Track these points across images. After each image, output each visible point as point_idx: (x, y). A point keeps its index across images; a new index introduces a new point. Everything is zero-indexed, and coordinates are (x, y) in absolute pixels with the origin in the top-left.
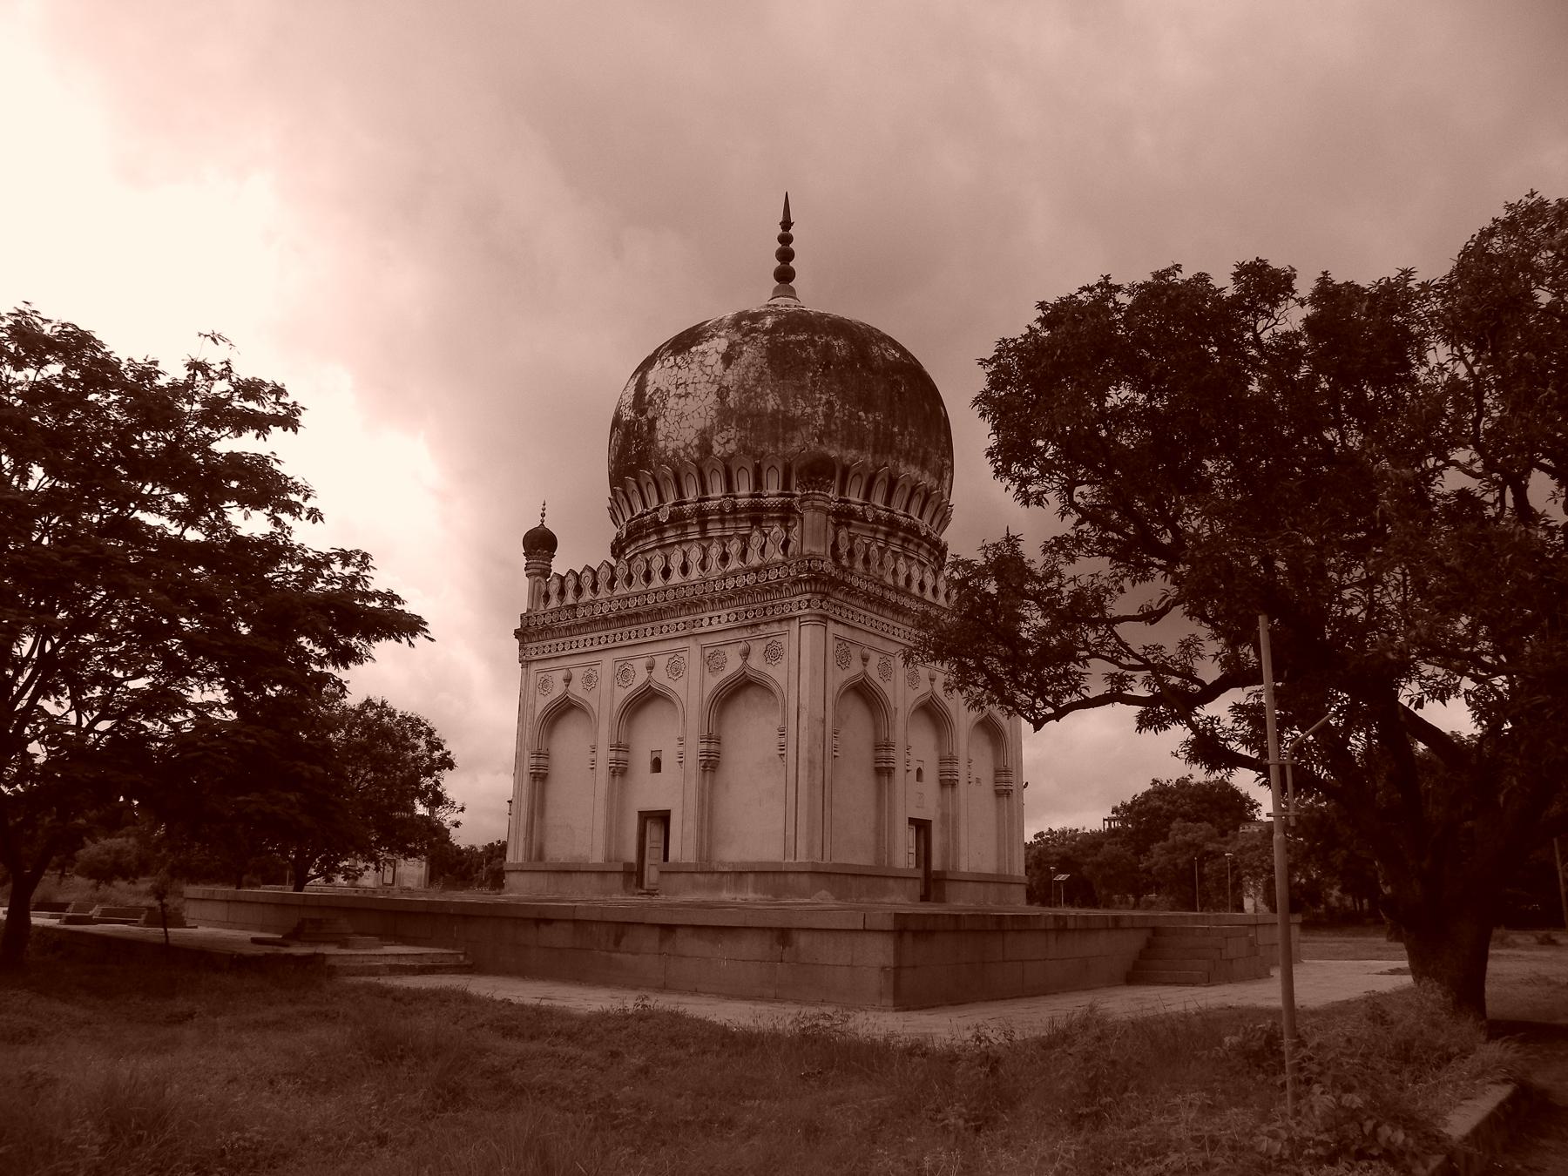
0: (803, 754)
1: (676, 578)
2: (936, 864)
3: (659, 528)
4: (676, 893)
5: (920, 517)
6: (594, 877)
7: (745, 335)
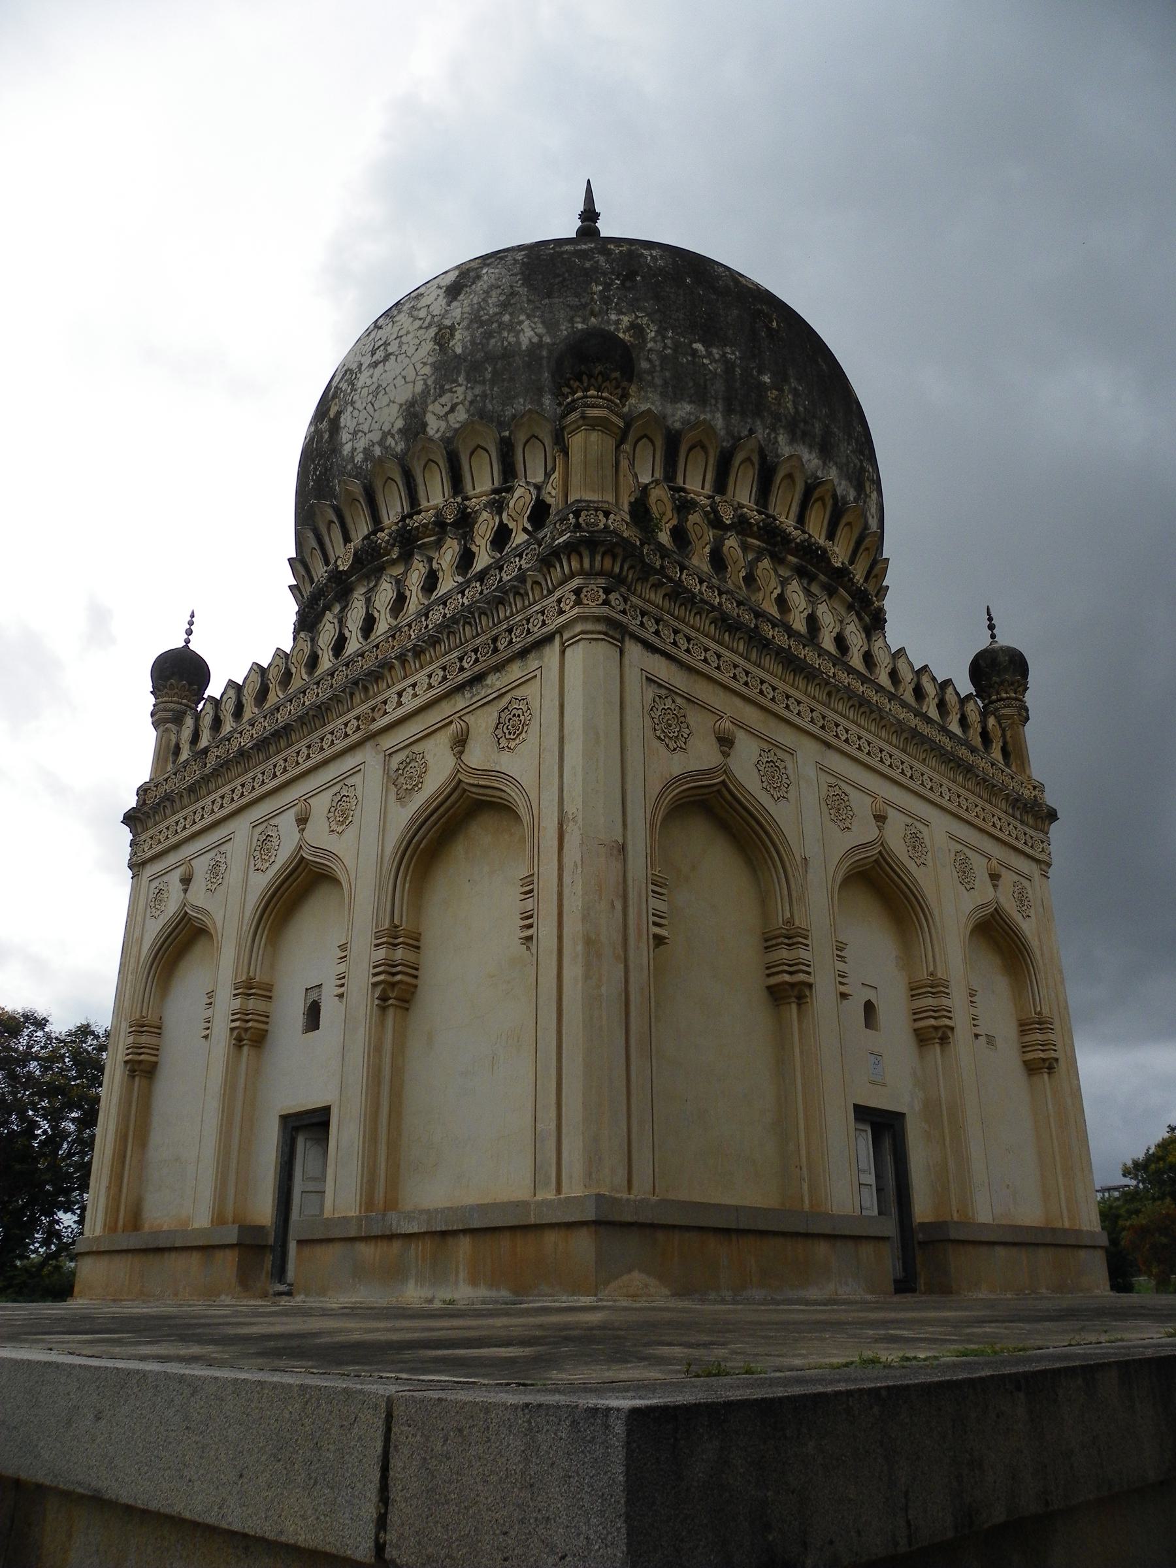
0: (573, 926)
2: (923, 1210)
4: (323, 1292)
5: (831, 536)
6: (195, 1258)
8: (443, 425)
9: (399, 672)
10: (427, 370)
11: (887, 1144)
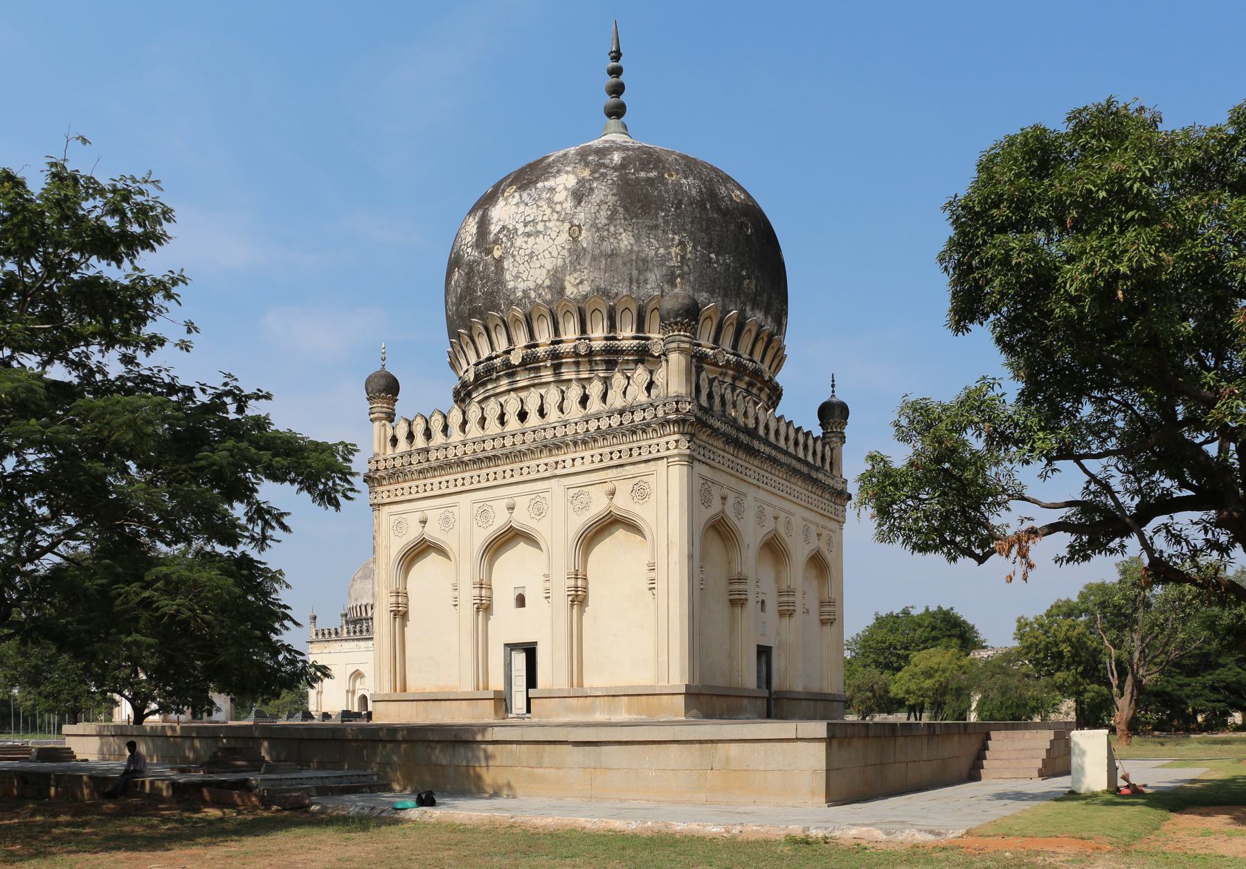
1: (533, 420)
3: (510, 371)
7: (593, 172)
9: (572, 448)
10: (566, 253)
11: (764, 658)
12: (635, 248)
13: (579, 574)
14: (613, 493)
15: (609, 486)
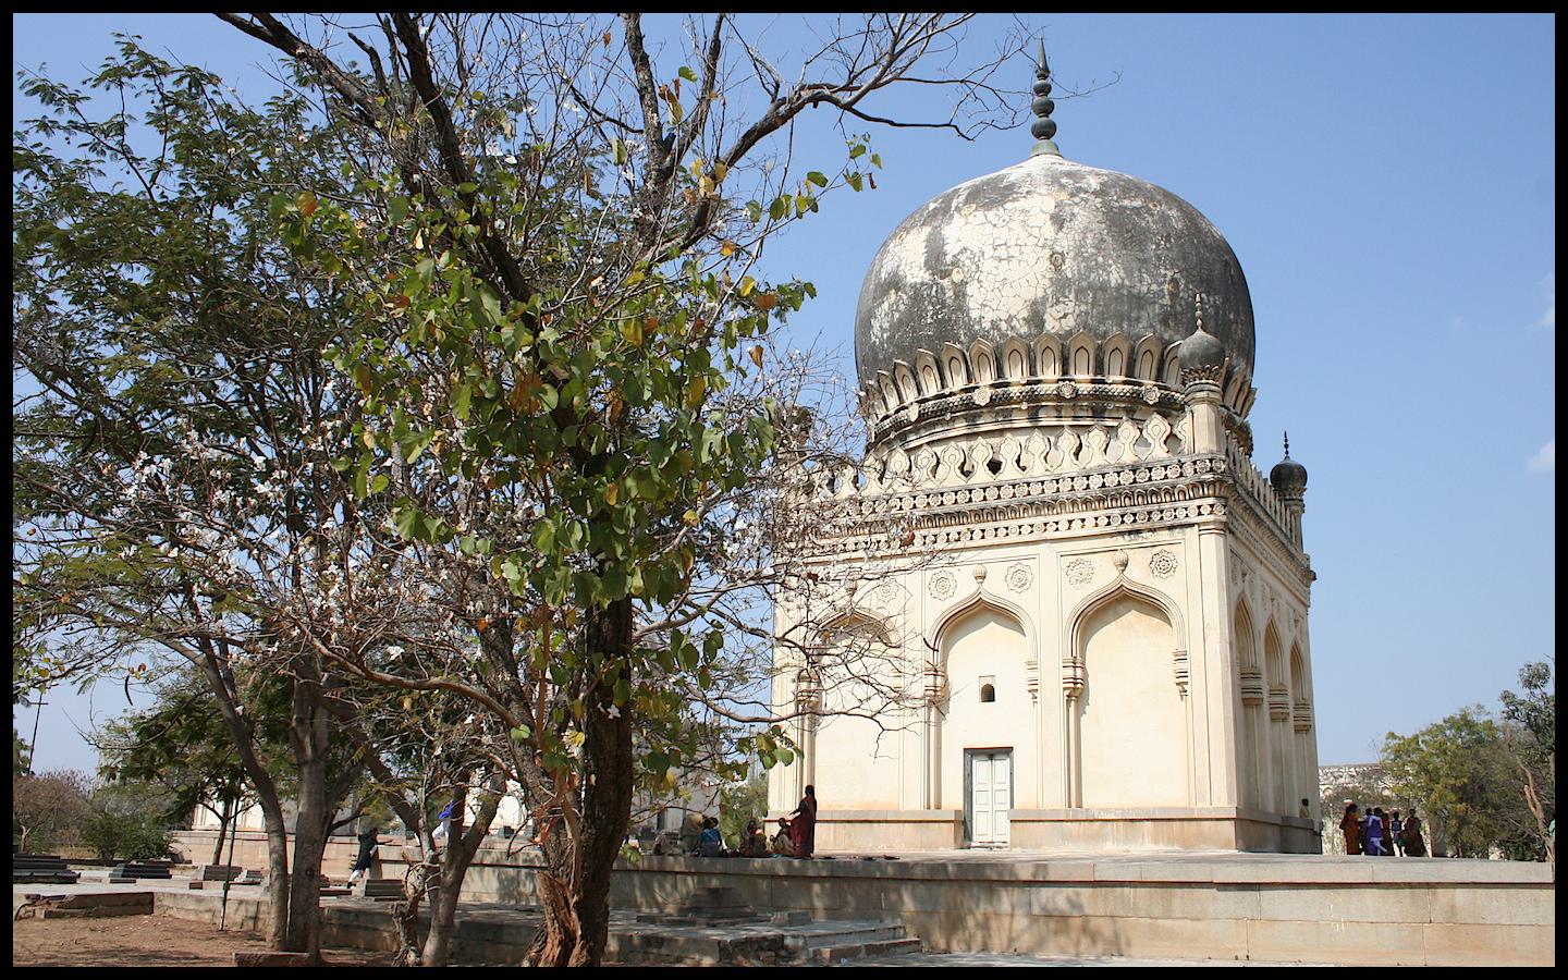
1: (1009, 472)
4: (1038, 847)
7: (1073, 195)
8: (1057, 325)
9: (1069, 507)
10: (1047, 282)
12: (1127, 283)
13: (1078, 662)
14: (1125, 565)
15: (1120, 556)
